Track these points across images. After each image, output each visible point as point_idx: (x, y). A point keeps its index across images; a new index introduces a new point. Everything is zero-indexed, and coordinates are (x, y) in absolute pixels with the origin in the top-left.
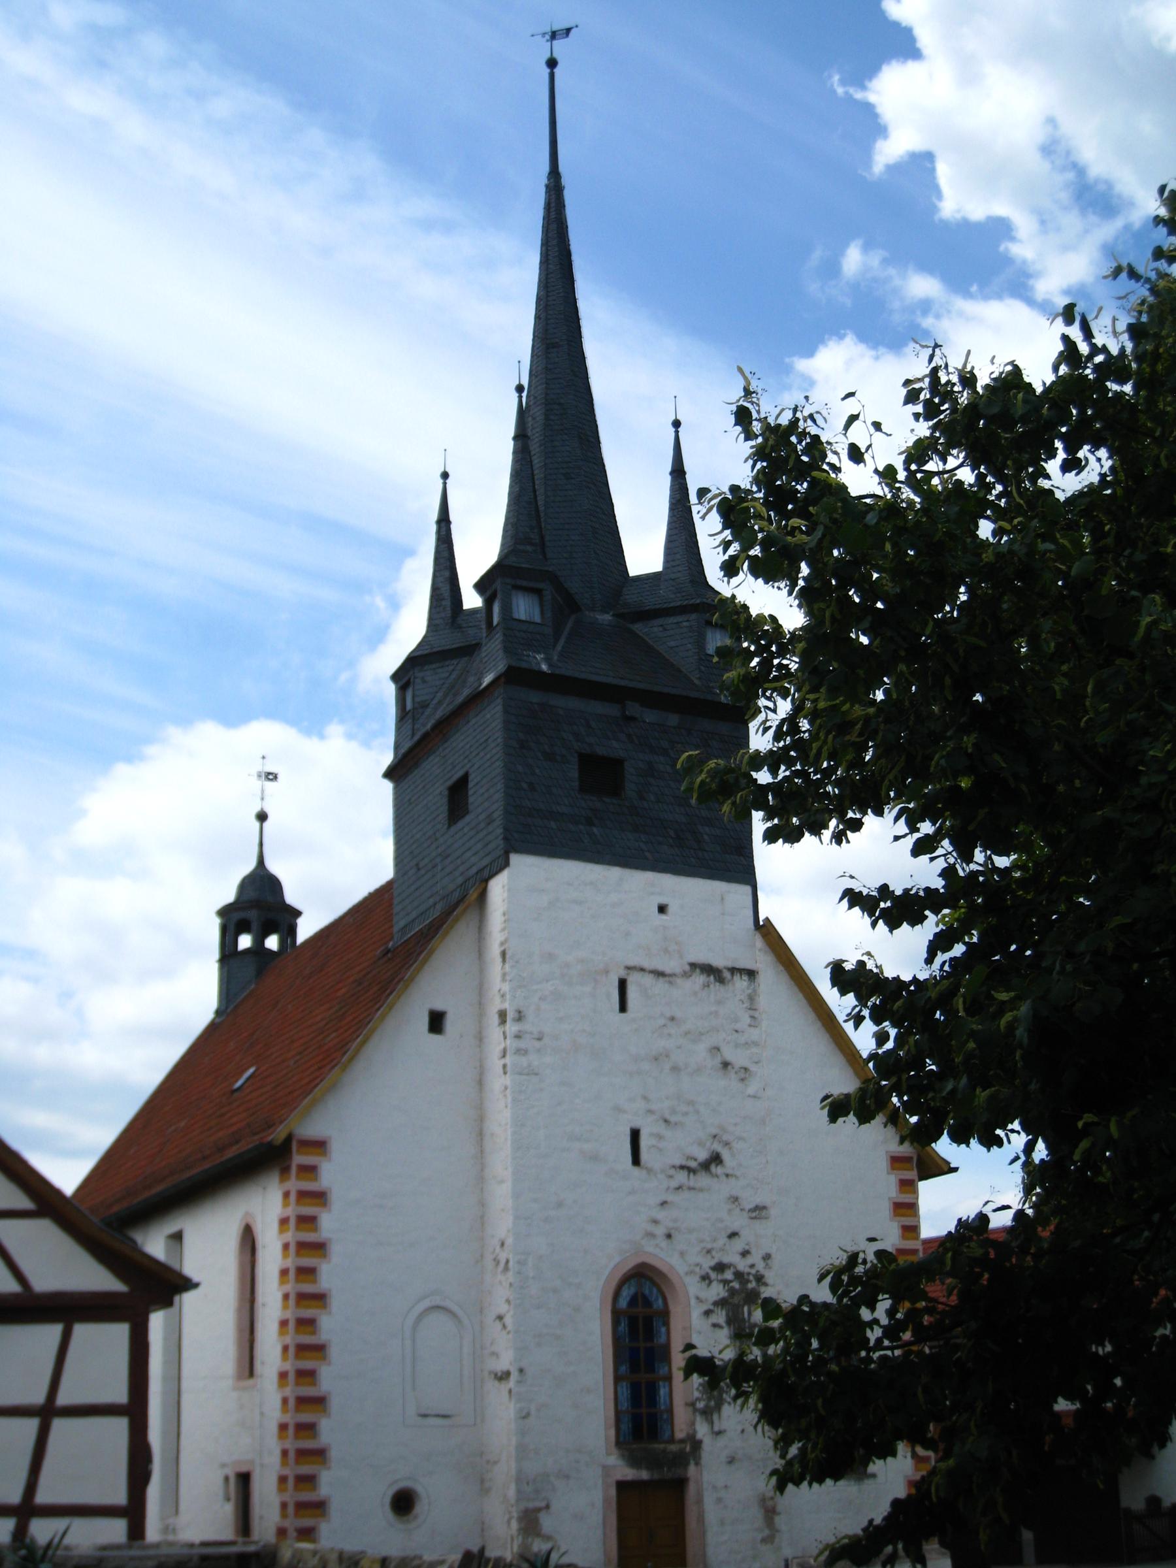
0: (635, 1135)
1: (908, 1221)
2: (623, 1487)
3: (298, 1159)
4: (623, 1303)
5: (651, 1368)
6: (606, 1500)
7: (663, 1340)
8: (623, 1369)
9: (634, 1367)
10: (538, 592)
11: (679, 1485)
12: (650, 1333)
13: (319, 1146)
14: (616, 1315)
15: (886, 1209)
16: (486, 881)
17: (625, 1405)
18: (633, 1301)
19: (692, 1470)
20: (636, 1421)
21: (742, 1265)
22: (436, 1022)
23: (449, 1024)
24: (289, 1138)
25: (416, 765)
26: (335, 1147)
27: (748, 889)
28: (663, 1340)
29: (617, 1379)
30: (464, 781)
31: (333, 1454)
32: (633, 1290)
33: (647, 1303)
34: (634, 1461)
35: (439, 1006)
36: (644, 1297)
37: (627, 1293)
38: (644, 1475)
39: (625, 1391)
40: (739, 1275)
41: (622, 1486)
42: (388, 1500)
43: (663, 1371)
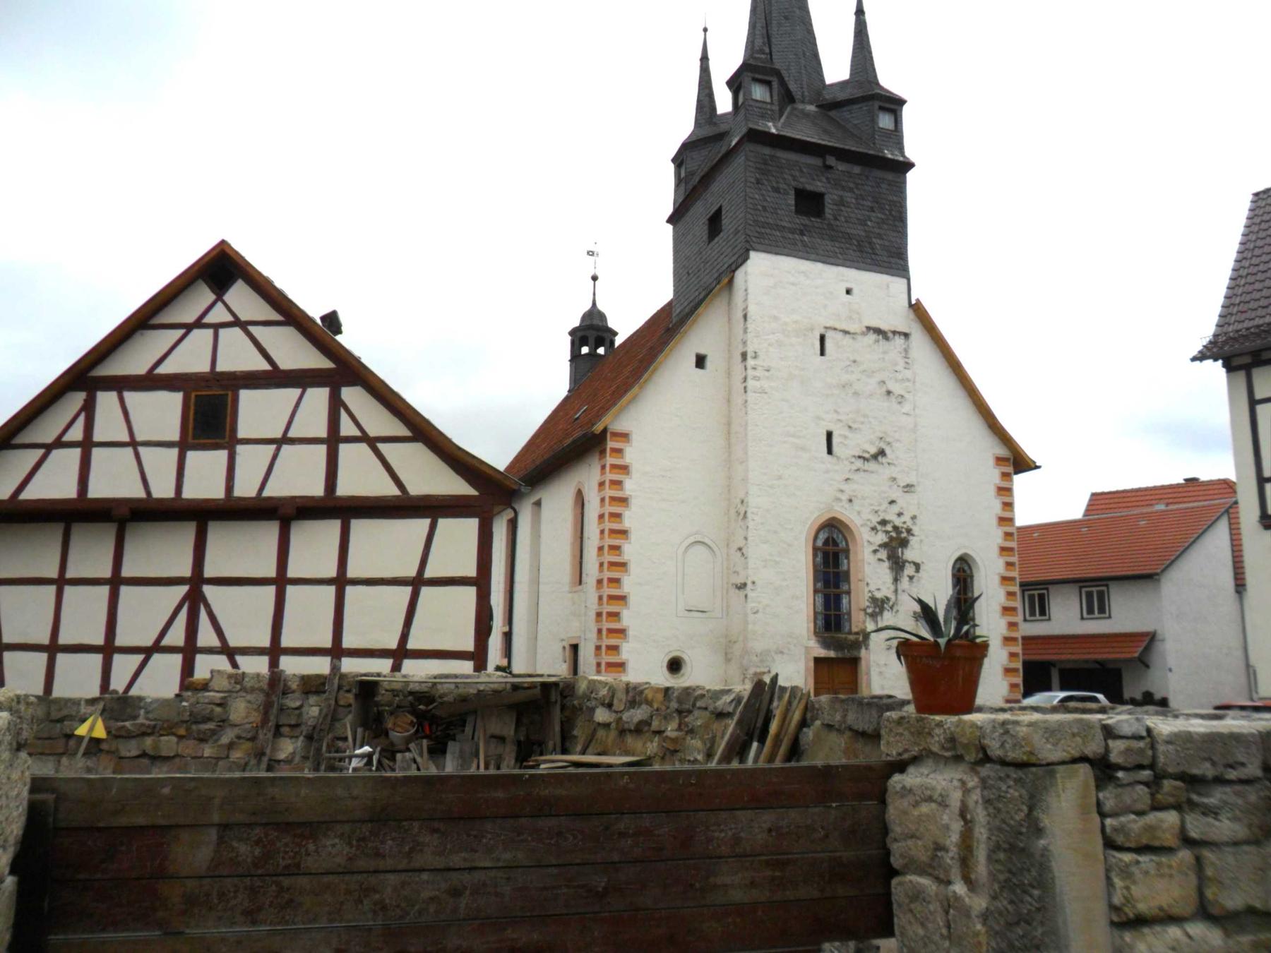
0: (829, 435)
1: (1007, 500)
2: (818, 661)
3: (611, 444)
4: (820, 543)
5: (837, 586)
6: (807, 669)
7: (845, 568)
8: (819, 585)
9: (827, 584)
10: (768, 83)
11: (854, 662)
12: (837, 563)
13: (625, 436)
14: (815, 549)
15: (992, 491)
16: (734, 271)
17: (820, 608)
18: (826, 542)
19: (863, 652)
20: (827, 619)
21: (898, 522)
22: (700, 361)
23: (708, 363)
24: (605, 431)
25: (687, 210)
26: (635, 437)
27: (905, 281)
28: (845, 568)
29: (816, 591)
30: (719, 211)
31: (631, 633)
32: (826, 535)
33: (835, 543)
34: (826, 644)
35: (702, 351)
36: (834, 540)
37: (822, 537)
38: (832, 654)
39: (820, 599)
40: (896, 528)
41: (818, 661)
42: (665, 664)
43: (845, 588)
